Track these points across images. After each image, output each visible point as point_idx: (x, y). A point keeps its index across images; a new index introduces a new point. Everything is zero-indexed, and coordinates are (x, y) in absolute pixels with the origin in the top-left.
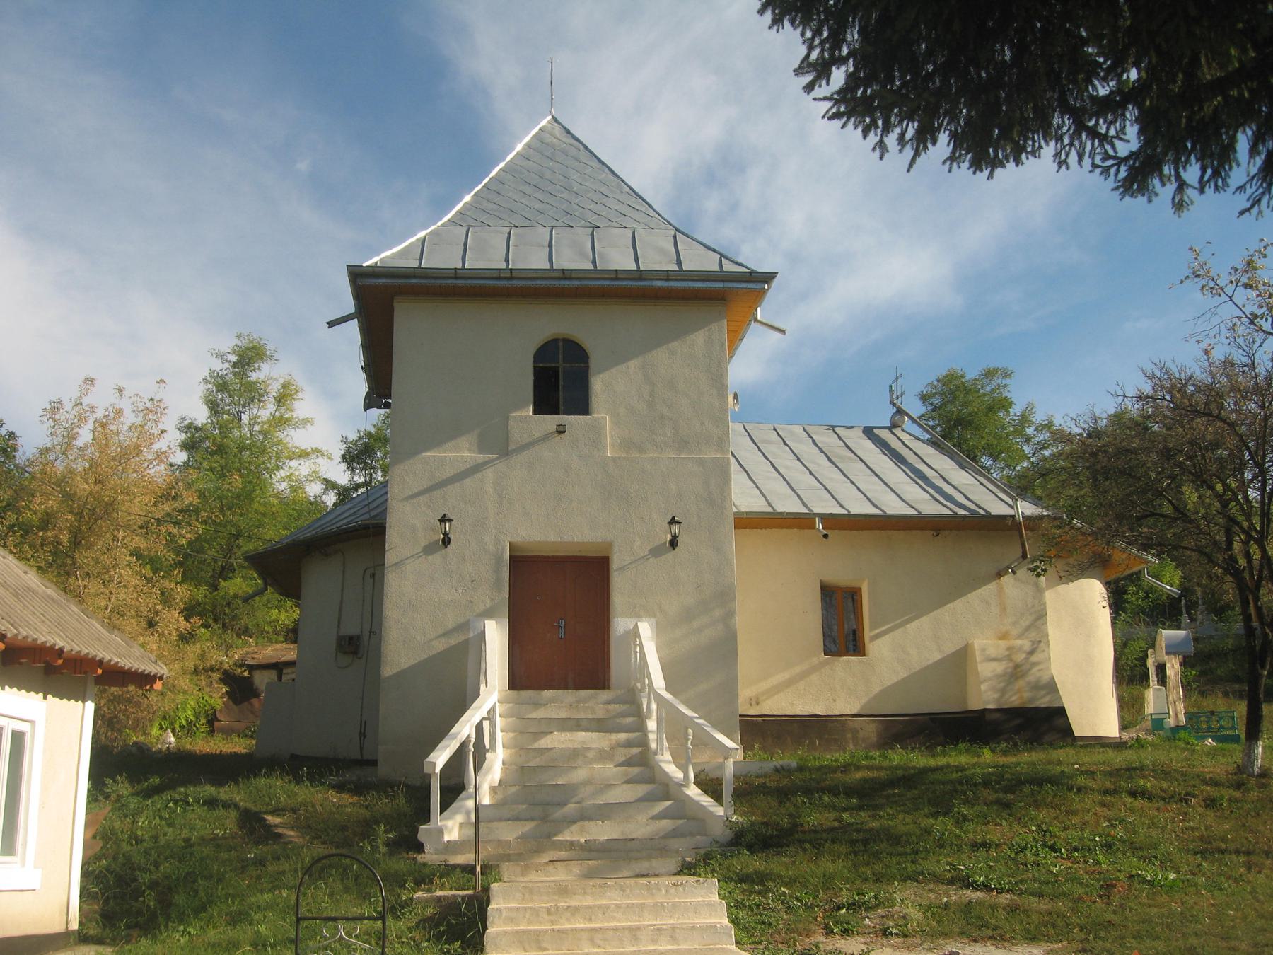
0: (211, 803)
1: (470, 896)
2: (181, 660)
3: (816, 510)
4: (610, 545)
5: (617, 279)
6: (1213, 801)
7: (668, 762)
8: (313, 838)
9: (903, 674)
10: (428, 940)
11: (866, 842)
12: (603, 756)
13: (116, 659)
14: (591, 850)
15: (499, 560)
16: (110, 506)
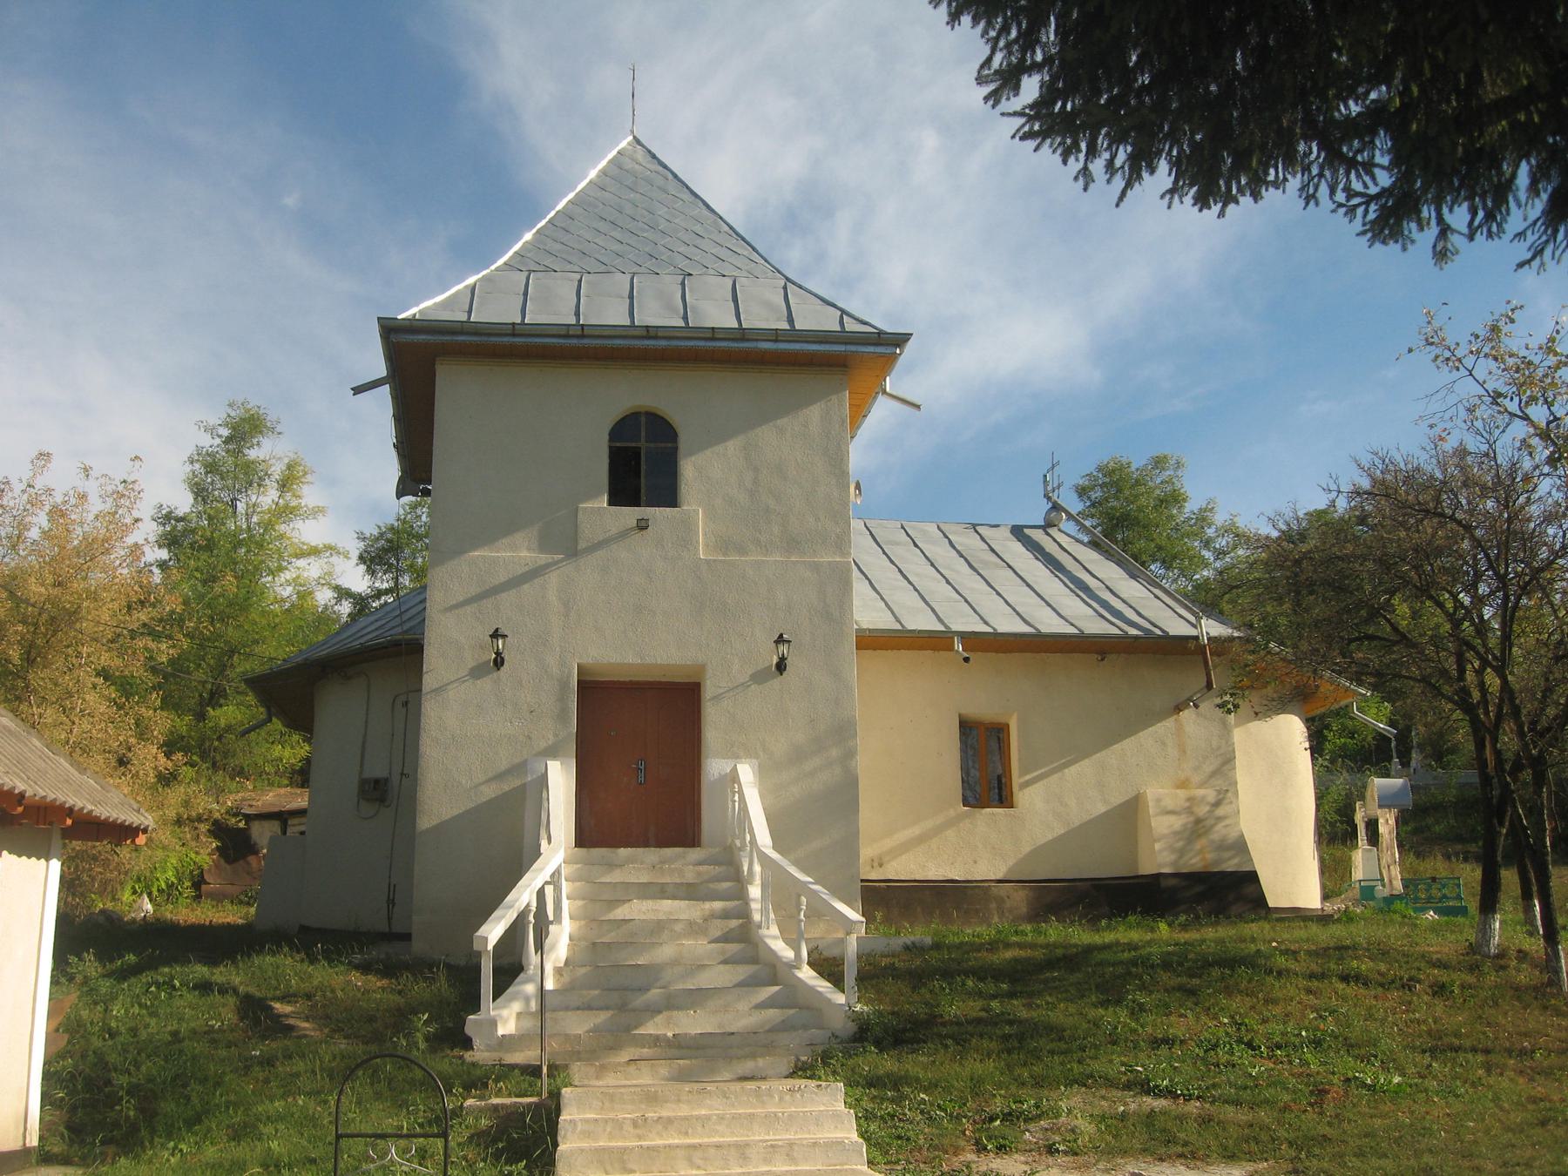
0: (204, 987)
1: (537, 1105)
2: (161, 806)
3: (955, 628)
4: (702, 668)
5: (713, 339)
6: (1443, 987)
7: (775, 937)
8: (334, 1031)
9: (1059, 830)
10: (484, 1160)
11: (1021, 1038)
12: (694, 929)
13: (90, 807)
14: (680, 1047)
15: (564, 685)
16: (73, 615)
